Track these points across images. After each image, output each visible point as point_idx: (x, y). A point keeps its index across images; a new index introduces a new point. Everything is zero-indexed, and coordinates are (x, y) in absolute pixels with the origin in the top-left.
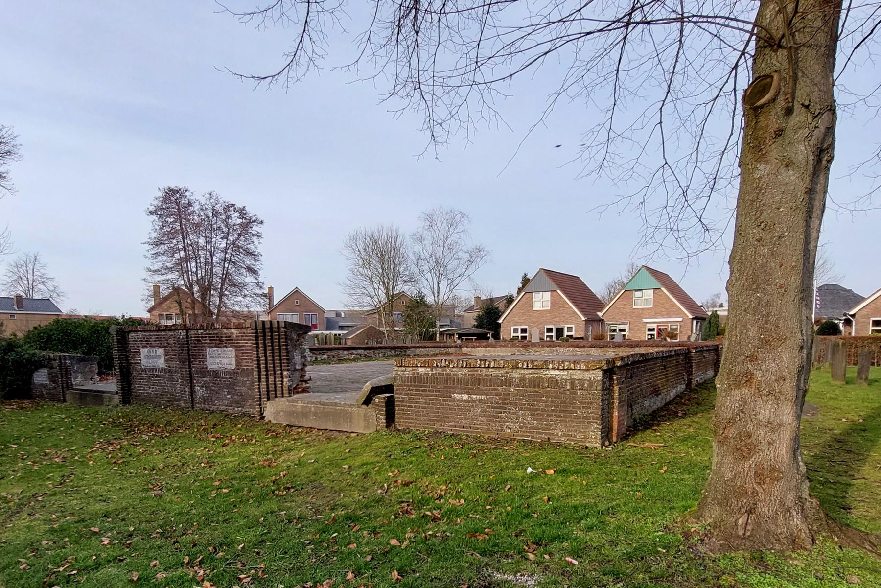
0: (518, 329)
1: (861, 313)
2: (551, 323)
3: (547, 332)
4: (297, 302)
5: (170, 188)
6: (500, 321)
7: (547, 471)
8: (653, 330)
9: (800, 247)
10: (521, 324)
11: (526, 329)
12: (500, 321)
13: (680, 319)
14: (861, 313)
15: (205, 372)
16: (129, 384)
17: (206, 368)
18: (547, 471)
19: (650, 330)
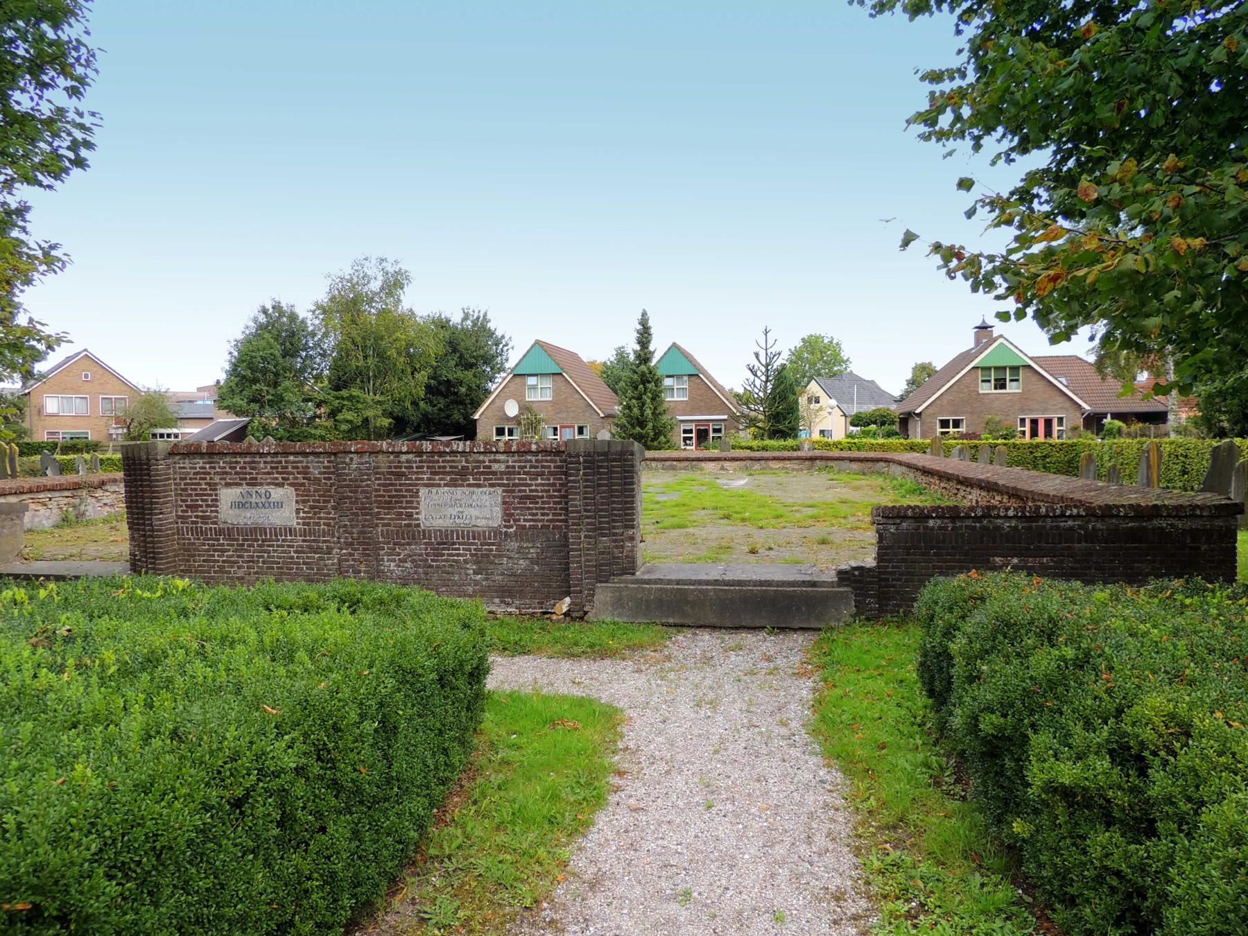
0: (948, 420)
1: (927, 412)
2: (1037, 411)
3: (954, 420)
4: (86, 376)
5: (319, 306)
6: (476, 417)
7: (1117, 184)
8: (690, 431)
9: (1058, 394)
10: (1055, 411)
11: (497, 429)
12: (476, 417)
13: (725, 417)
14: (927, 412)
15: (413, 533)
16: (981, 488)
17: (418, 525)
18: (1117, 184)
19: (685, 431)
